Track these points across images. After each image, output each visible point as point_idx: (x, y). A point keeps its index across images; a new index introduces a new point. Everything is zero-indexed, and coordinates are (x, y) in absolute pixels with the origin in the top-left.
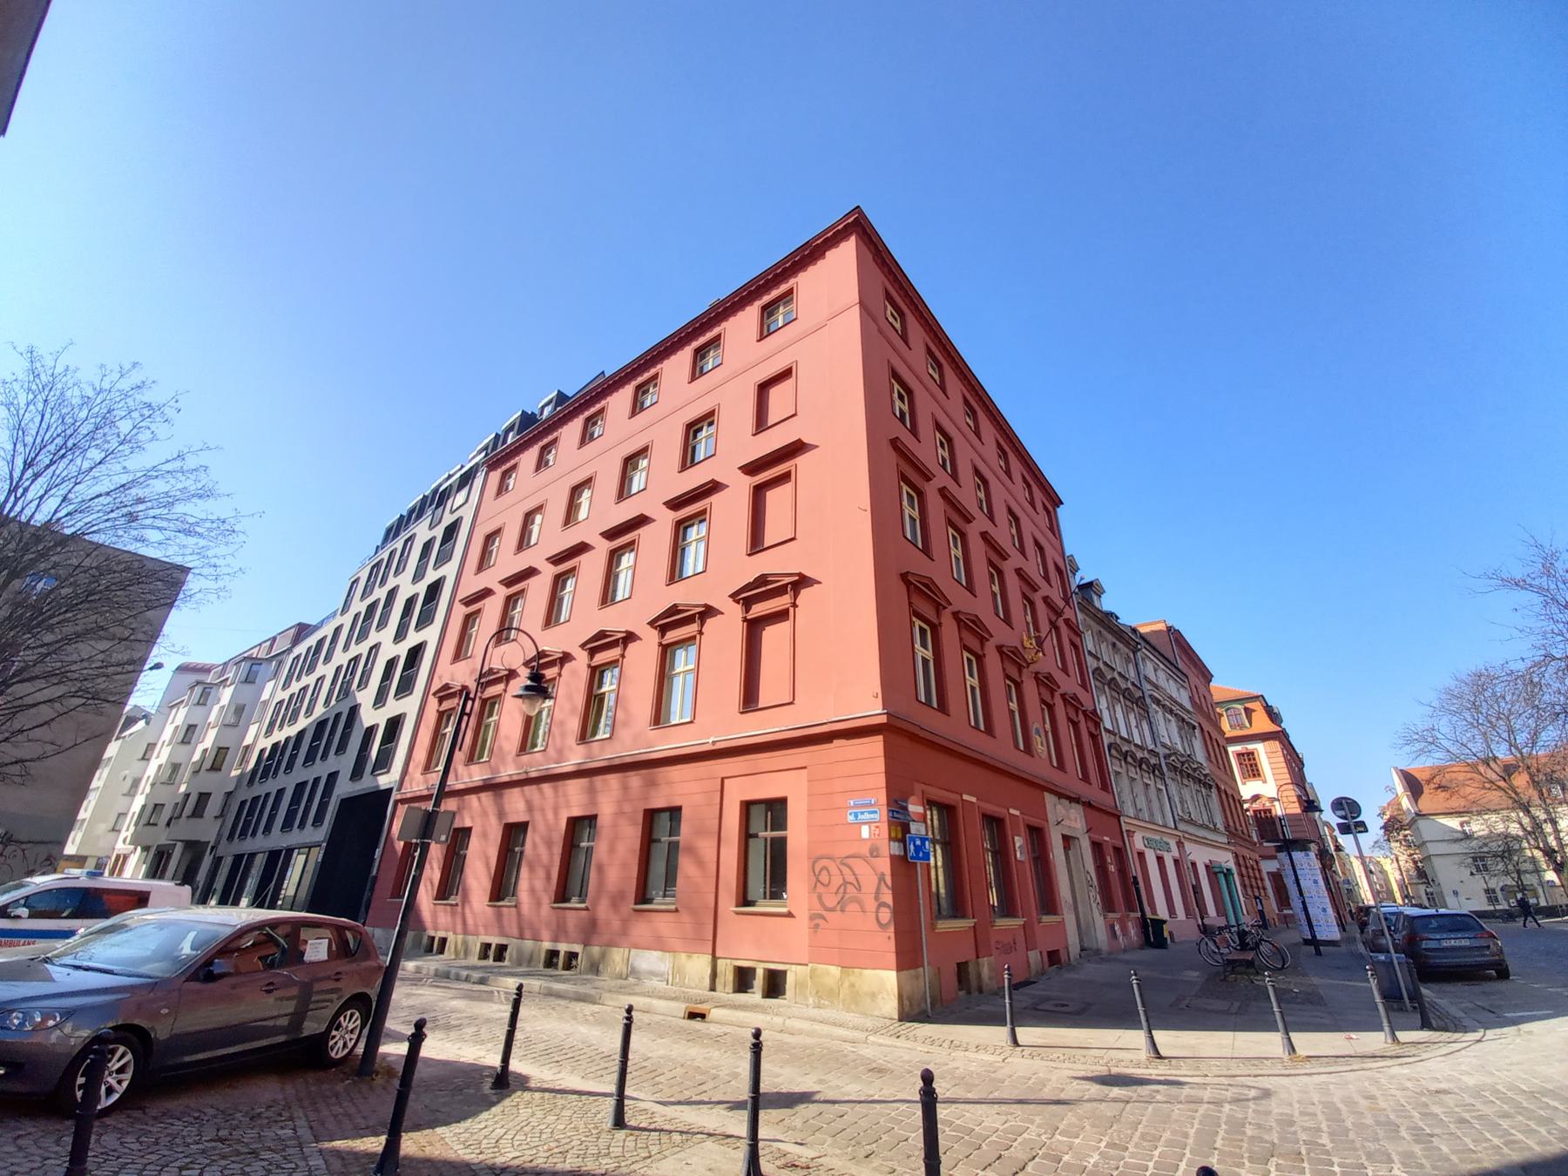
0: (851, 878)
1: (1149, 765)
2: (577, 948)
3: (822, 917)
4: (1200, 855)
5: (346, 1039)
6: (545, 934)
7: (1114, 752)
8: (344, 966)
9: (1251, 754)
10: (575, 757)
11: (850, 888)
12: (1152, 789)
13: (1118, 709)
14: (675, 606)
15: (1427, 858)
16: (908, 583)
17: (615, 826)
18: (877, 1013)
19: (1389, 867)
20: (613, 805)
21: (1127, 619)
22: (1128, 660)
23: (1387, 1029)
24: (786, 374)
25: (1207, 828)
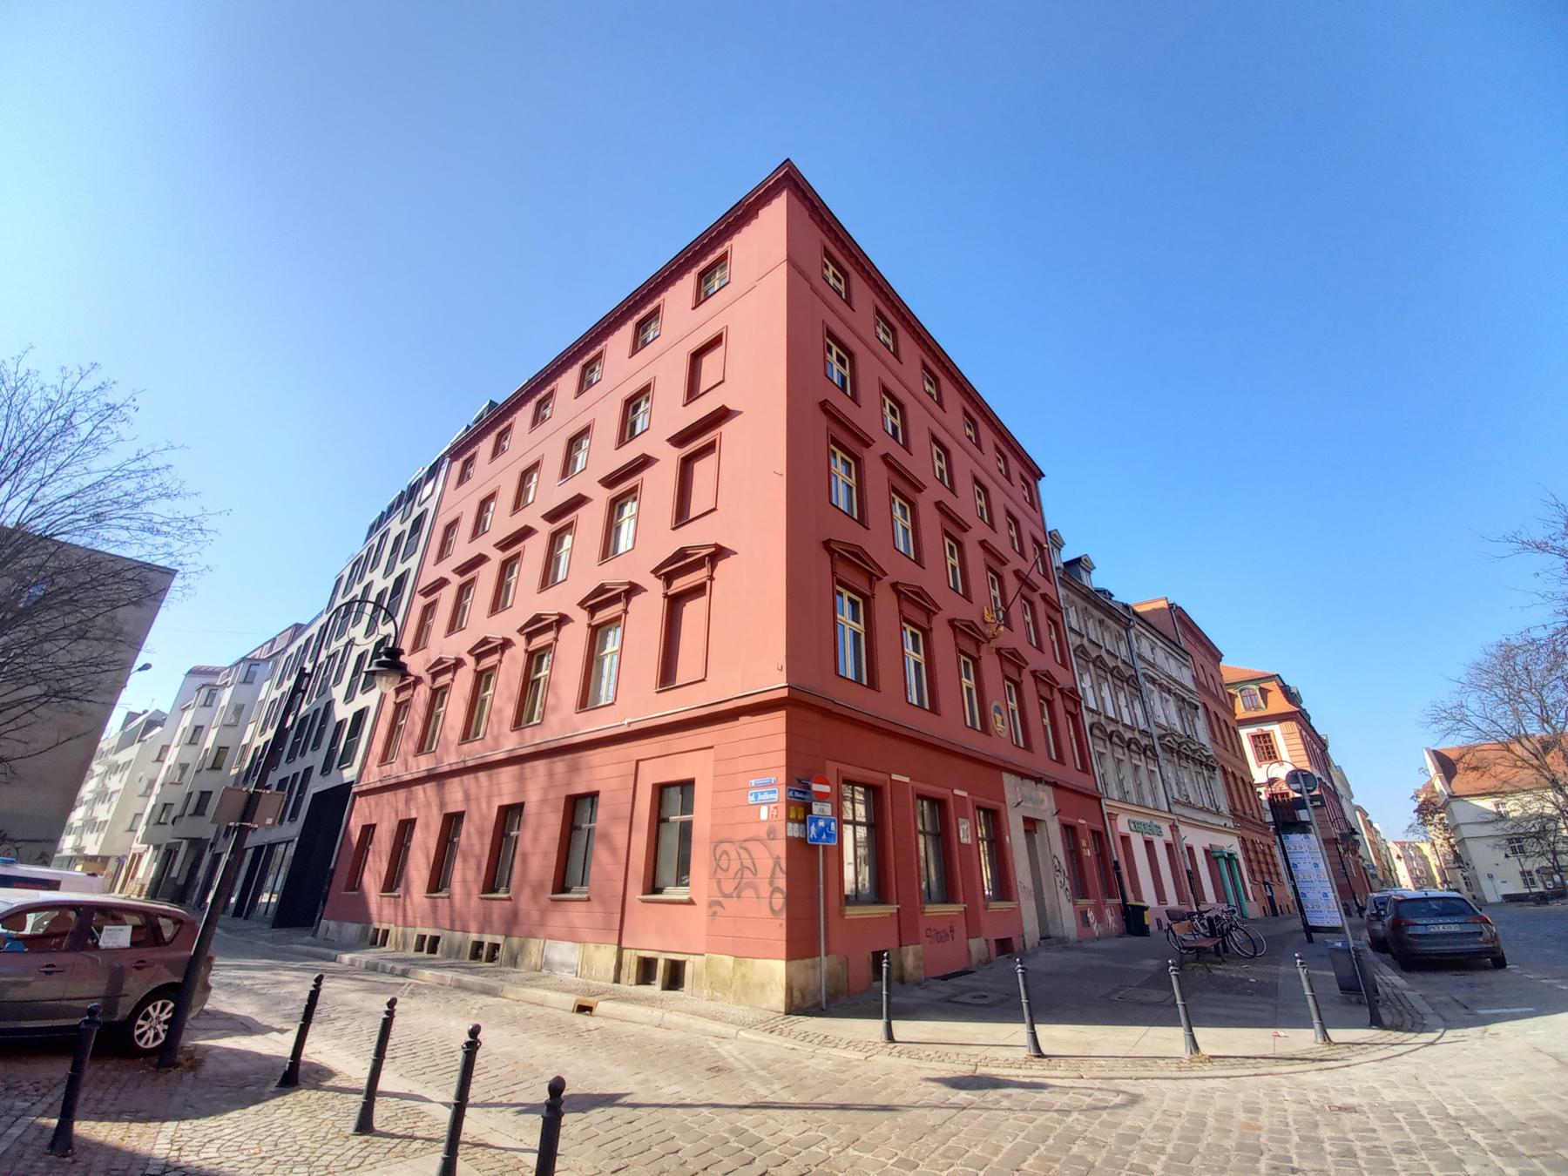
0: (748, 863)
1: (1142, 746)
2: (499, 939)
3: (720, 904)
4: (1198, 840)
5: (151, 1030)
6: (473, 926)
7: (1097, 732)
8: (144, 953)
9: (1266, 736)
10: (510, 743)
11: (747, 874)
12: (1143, 774)
13: (1105, 687)
14: (602, 585)
15: (1461, 842)
16: (831, 552)
17: (539, 814)
18: (765, 1006)
19: (1426, 849)
20: (540, 791)
21: (1121, 596)
22: (1119, 637)
23: (1317, 1026)
24: (716, 342)
25: (1208, 811)
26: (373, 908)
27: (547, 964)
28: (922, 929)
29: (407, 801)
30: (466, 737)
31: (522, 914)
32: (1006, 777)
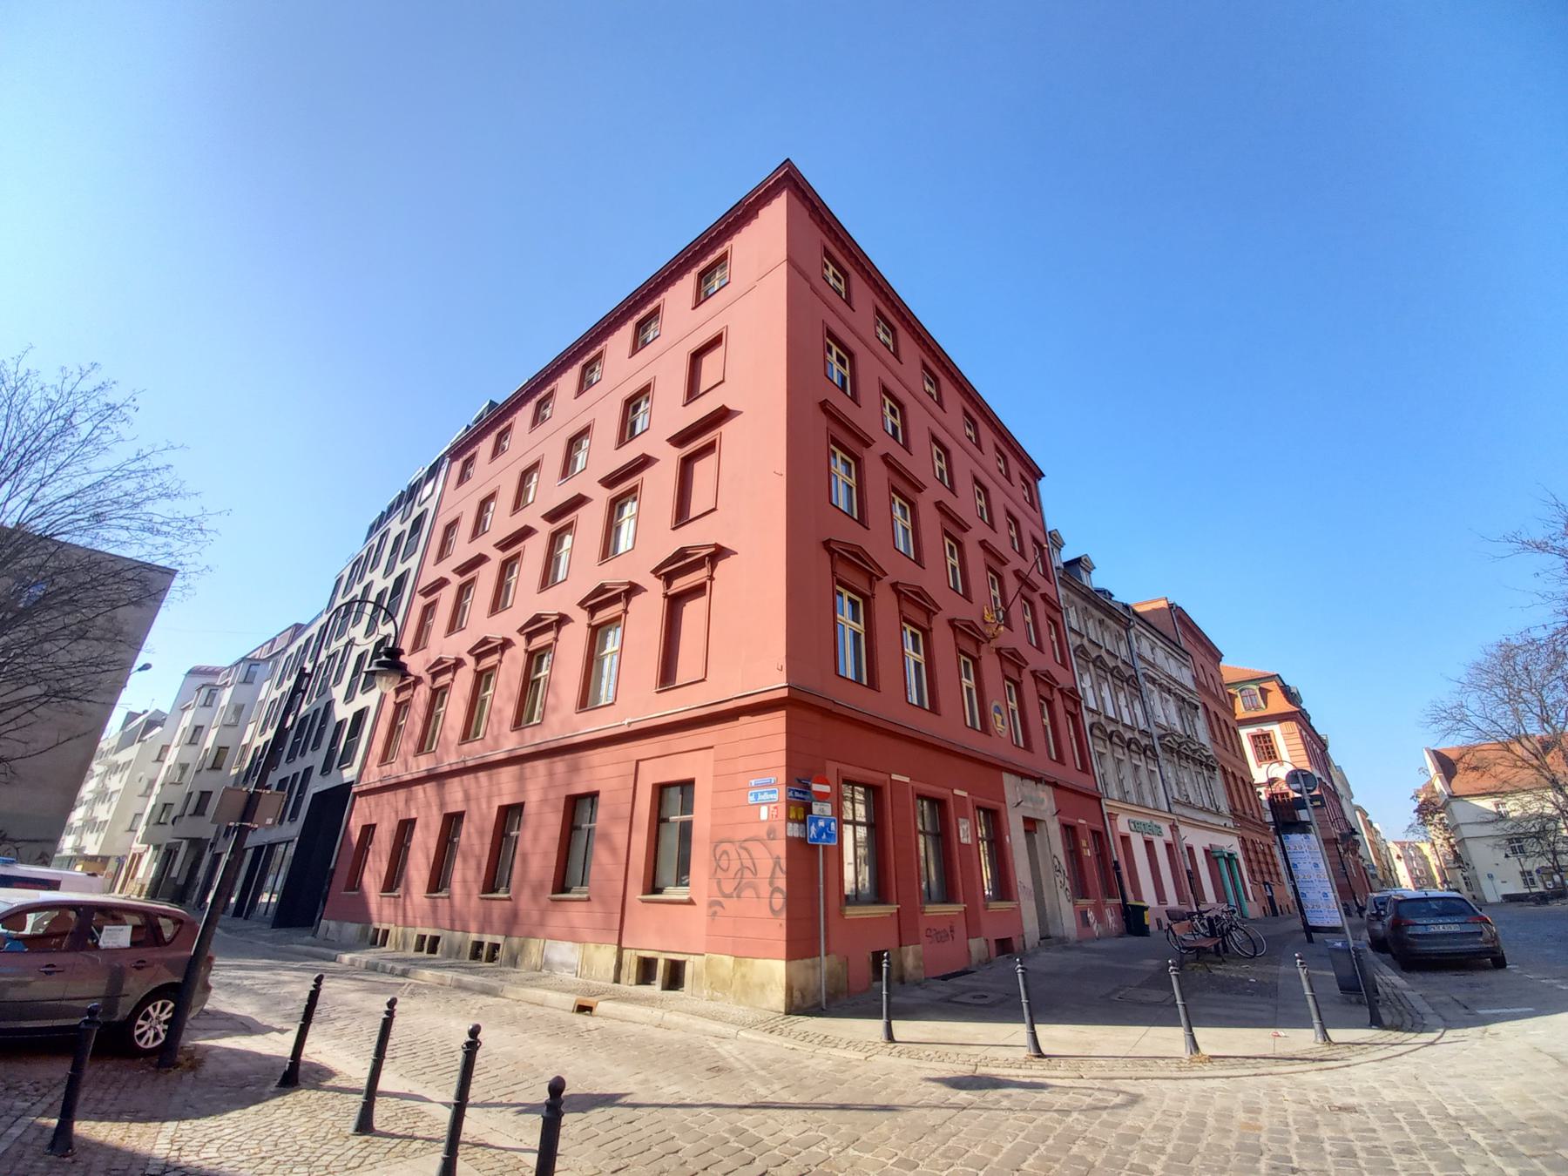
0: (748, 863)
1: (1142, 746)
2: (499, 939)
3: (720, 904)
4: (1198, 840)
5: (151, 1030)
6: (473, 926)
7: (1097, 732)
8: (144, 953)
9: (1266, 736)
10: (510, 743)
11: (747, 874)
12: (1143, 774)
13: (1105, 687)
14: (602, 585)
15: (1461, 842)
16: (831, 552)
17: (539, 814)
18: (765, 1006)
19: (1426, 849)
20: (540, 791)
21: (1121, 596)
22: (1119, 637)
23: (1317, 1026)
24: (716, 342)
25: (1208, 811)
26: (373, 908)
27: (547, 964)
28: (922, 929)
29: (407, 801)
30: (466, 737)
31: (522, 914)
32: (1006, 777)
